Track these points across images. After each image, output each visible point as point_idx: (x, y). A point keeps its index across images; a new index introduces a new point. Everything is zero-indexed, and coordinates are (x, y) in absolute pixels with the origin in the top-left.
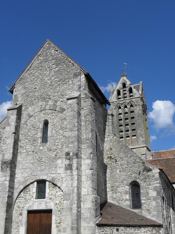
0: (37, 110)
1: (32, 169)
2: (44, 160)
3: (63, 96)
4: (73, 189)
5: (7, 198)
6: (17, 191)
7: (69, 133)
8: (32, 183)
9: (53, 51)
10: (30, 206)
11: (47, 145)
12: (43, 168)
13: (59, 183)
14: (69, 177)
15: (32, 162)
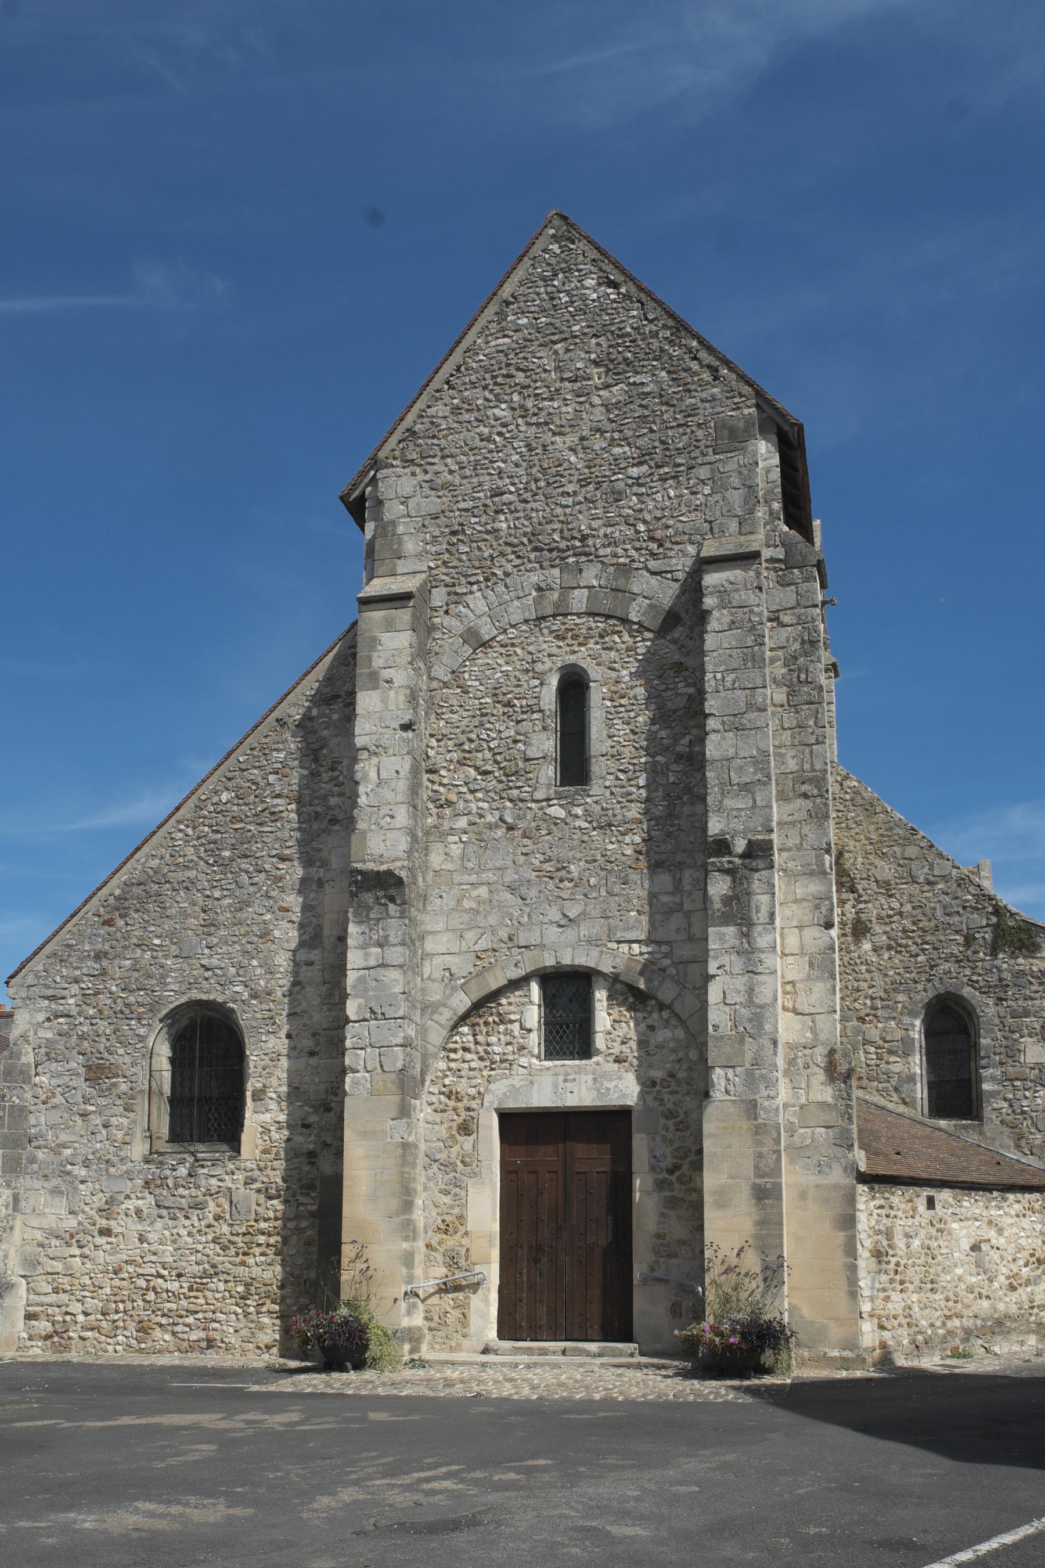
0: (516, 612)
2: (575, 875)
6: (436, 1017)
8: (514, 985)
9: (590, 282)
10: (514, 1090)
11: (589, 800)
15: (510, 876)
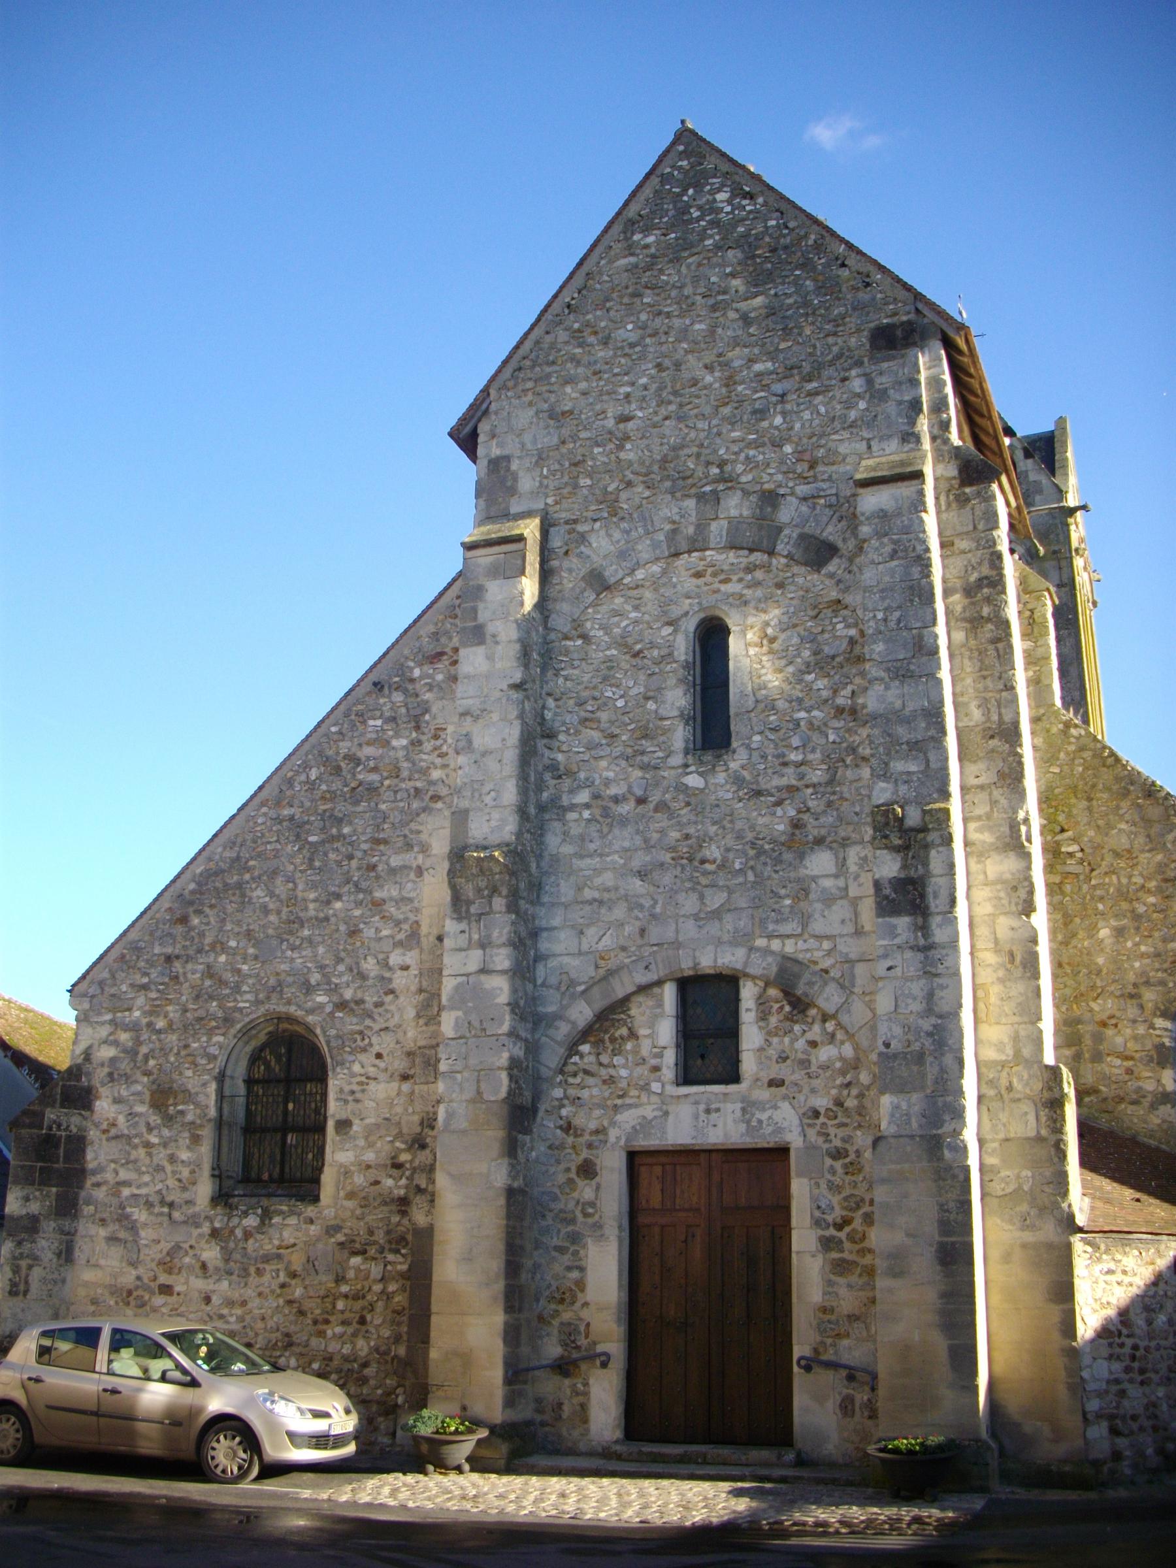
1: (641, 907)
3: (812, 465)
4: (935, 1026)
5: (504, 1076)
7: (887, 688)
10: (645, 1125)
13: (831, 988)
14: (909, 954)
15: (639, 860)
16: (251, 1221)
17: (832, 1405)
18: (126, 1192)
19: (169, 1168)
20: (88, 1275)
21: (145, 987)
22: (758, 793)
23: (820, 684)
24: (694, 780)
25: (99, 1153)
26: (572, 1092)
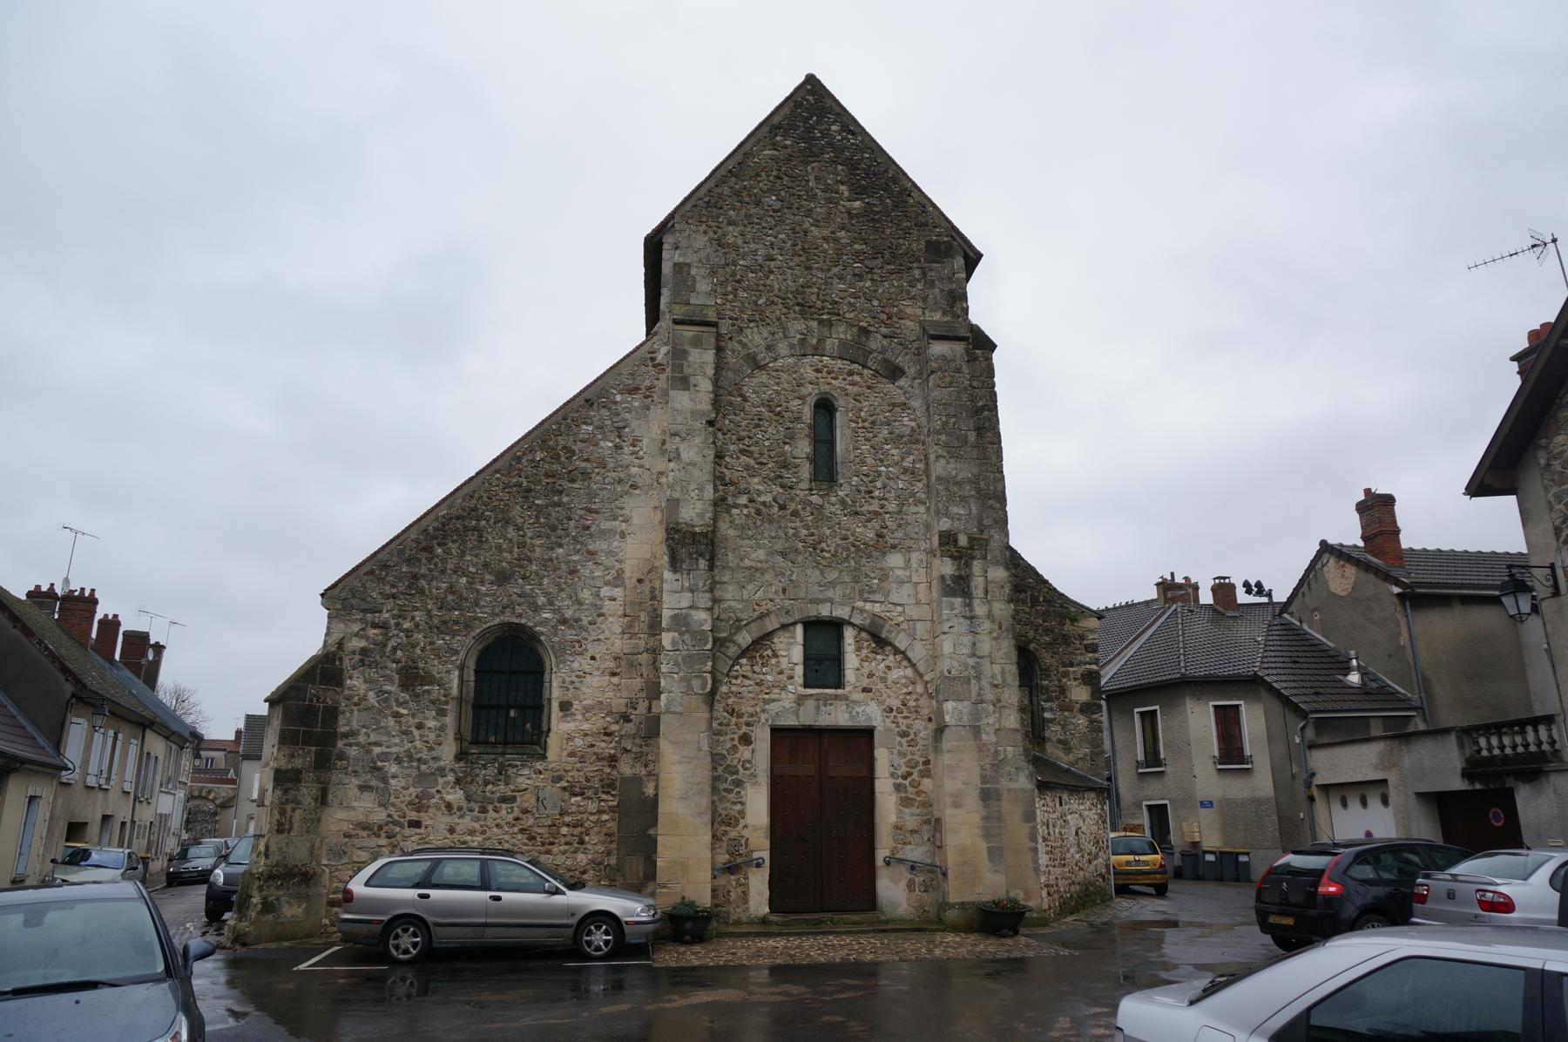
9: (834, 128)
12: (833, 575)
13: (902, 635)
15: (779, 546)
16: (491, 771)
17: (903, 884)
18: (377, 750)
19: (416, 733)
20: (341, 814)
21: (394, 597)
22: (857, 513)
23: (894, 452)
24: (815, 499)
25: (350, 720)
26: (734, 689)
